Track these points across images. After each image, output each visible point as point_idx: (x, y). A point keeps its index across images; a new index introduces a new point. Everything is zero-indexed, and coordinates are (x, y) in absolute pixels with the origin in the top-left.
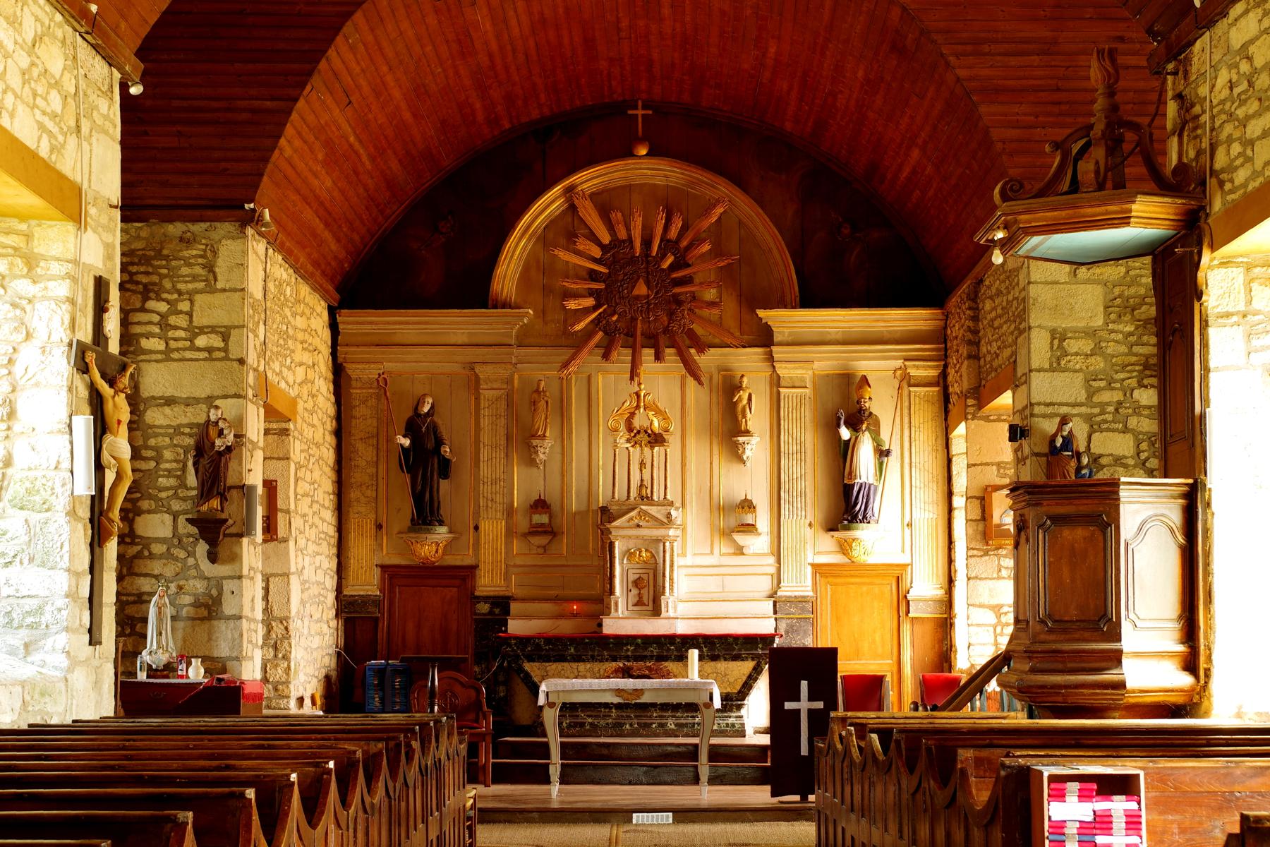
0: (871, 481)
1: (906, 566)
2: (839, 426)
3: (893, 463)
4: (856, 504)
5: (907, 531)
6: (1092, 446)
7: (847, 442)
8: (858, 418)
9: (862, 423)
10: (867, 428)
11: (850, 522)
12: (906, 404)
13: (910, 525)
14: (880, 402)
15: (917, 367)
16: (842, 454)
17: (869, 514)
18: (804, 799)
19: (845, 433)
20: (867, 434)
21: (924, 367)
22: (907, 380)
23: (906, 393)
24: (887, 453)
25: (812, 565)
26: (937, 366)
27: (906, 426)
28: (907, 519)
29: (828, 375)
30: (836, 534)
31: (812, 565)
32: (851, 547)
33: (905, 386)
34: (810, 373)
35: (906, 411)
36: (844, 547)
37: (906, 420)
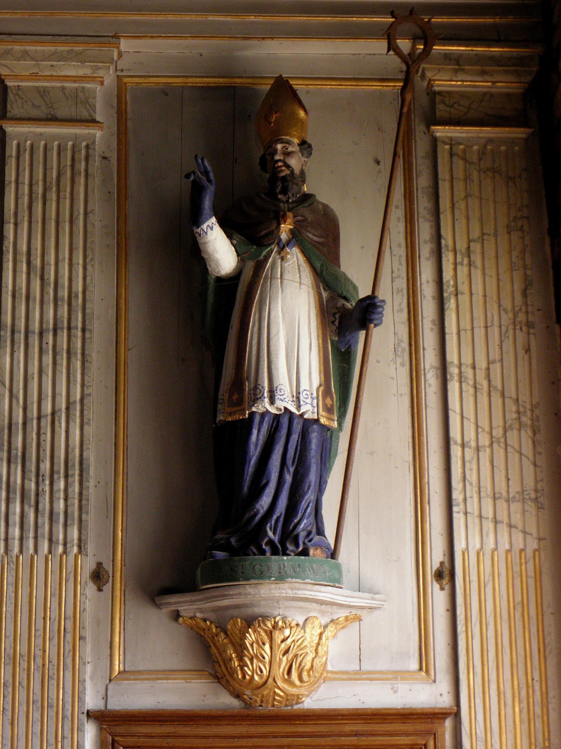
0: (309, 409)
1: (431, 717)
2: (196, 219)
3: (384, 342)
4: (257, 489)
5: (439, 598)
6: (108, 706)
7: (233, 279)
8: (264, 207)
9: (279, 218)
10: (296, 237)
11: (234, 552)
12: (422, 181)
13: (446, 574)
14: (339, 169)
15: (457, 63)
16: (212, 326)
17: (305, 525)
18: (430, 20)
19: (221, 252)
20: (295, 256)
21: (478, 60)
22: (417, 112)
23: (421, 147)
24: (366, 313)
25: (101, 718)
26: (520, 61)
27: (425, 250)
28: (436, 555)
29: (165, 91)
30: (190, 606)
31: (101, 718)
32: (241, 649)
33: (419, 128)
34: (109, 78)
35: (423, 204)
36: (216, 651)
37: (424, 230)
